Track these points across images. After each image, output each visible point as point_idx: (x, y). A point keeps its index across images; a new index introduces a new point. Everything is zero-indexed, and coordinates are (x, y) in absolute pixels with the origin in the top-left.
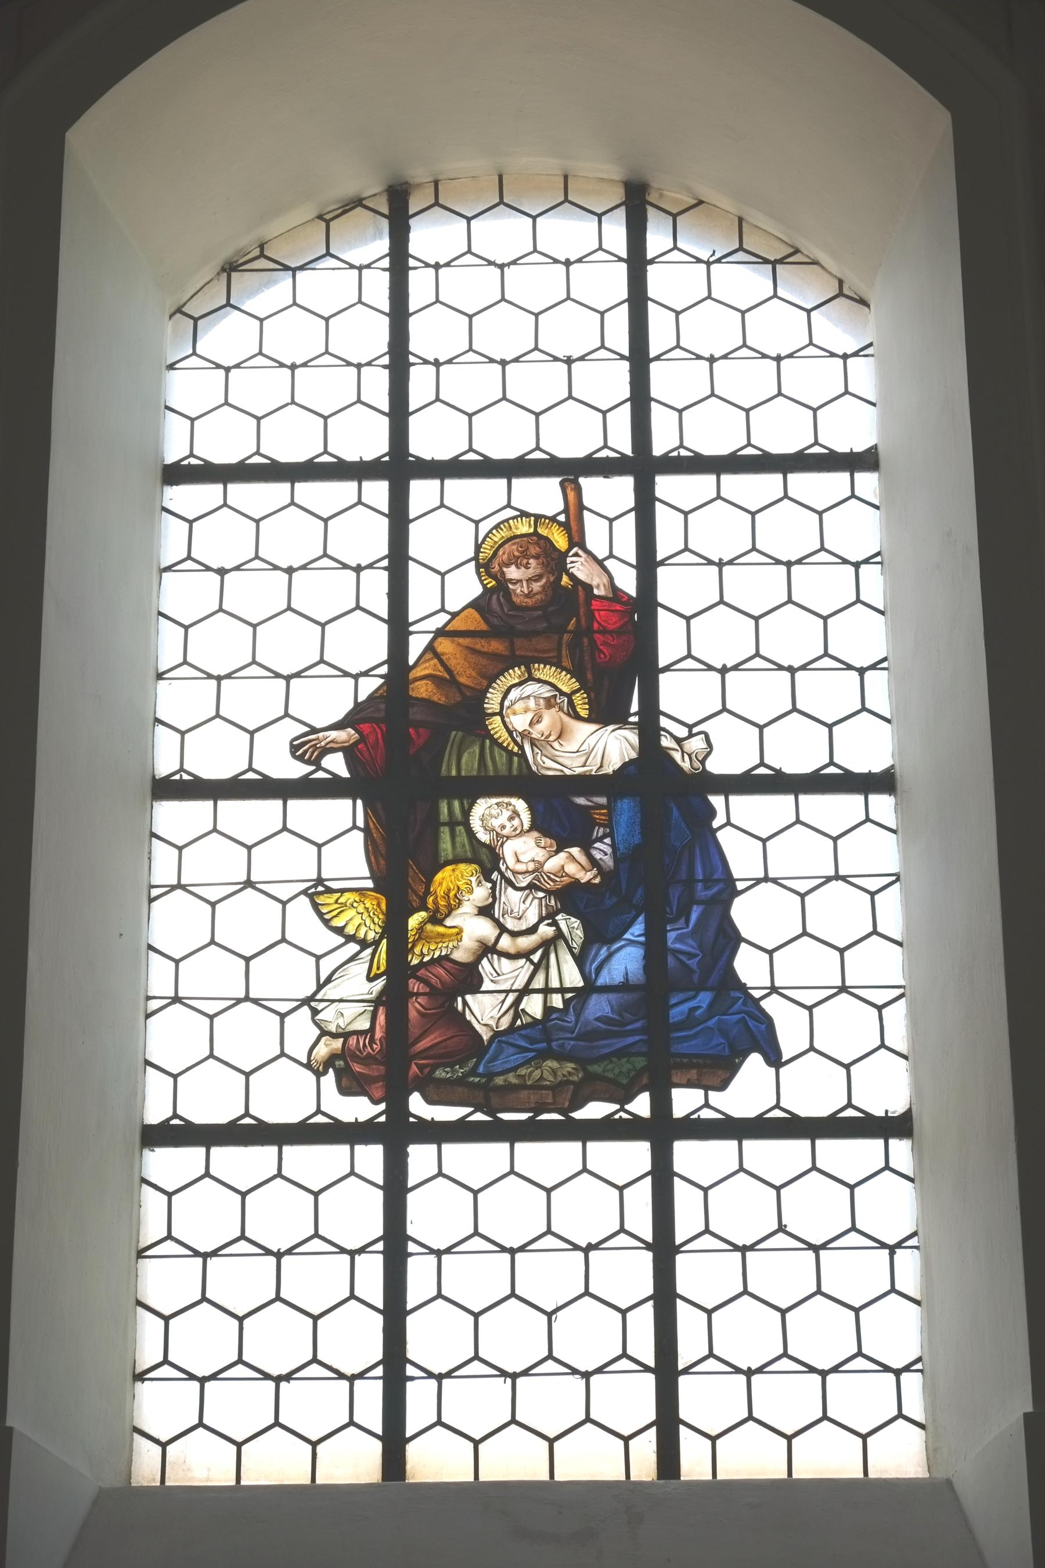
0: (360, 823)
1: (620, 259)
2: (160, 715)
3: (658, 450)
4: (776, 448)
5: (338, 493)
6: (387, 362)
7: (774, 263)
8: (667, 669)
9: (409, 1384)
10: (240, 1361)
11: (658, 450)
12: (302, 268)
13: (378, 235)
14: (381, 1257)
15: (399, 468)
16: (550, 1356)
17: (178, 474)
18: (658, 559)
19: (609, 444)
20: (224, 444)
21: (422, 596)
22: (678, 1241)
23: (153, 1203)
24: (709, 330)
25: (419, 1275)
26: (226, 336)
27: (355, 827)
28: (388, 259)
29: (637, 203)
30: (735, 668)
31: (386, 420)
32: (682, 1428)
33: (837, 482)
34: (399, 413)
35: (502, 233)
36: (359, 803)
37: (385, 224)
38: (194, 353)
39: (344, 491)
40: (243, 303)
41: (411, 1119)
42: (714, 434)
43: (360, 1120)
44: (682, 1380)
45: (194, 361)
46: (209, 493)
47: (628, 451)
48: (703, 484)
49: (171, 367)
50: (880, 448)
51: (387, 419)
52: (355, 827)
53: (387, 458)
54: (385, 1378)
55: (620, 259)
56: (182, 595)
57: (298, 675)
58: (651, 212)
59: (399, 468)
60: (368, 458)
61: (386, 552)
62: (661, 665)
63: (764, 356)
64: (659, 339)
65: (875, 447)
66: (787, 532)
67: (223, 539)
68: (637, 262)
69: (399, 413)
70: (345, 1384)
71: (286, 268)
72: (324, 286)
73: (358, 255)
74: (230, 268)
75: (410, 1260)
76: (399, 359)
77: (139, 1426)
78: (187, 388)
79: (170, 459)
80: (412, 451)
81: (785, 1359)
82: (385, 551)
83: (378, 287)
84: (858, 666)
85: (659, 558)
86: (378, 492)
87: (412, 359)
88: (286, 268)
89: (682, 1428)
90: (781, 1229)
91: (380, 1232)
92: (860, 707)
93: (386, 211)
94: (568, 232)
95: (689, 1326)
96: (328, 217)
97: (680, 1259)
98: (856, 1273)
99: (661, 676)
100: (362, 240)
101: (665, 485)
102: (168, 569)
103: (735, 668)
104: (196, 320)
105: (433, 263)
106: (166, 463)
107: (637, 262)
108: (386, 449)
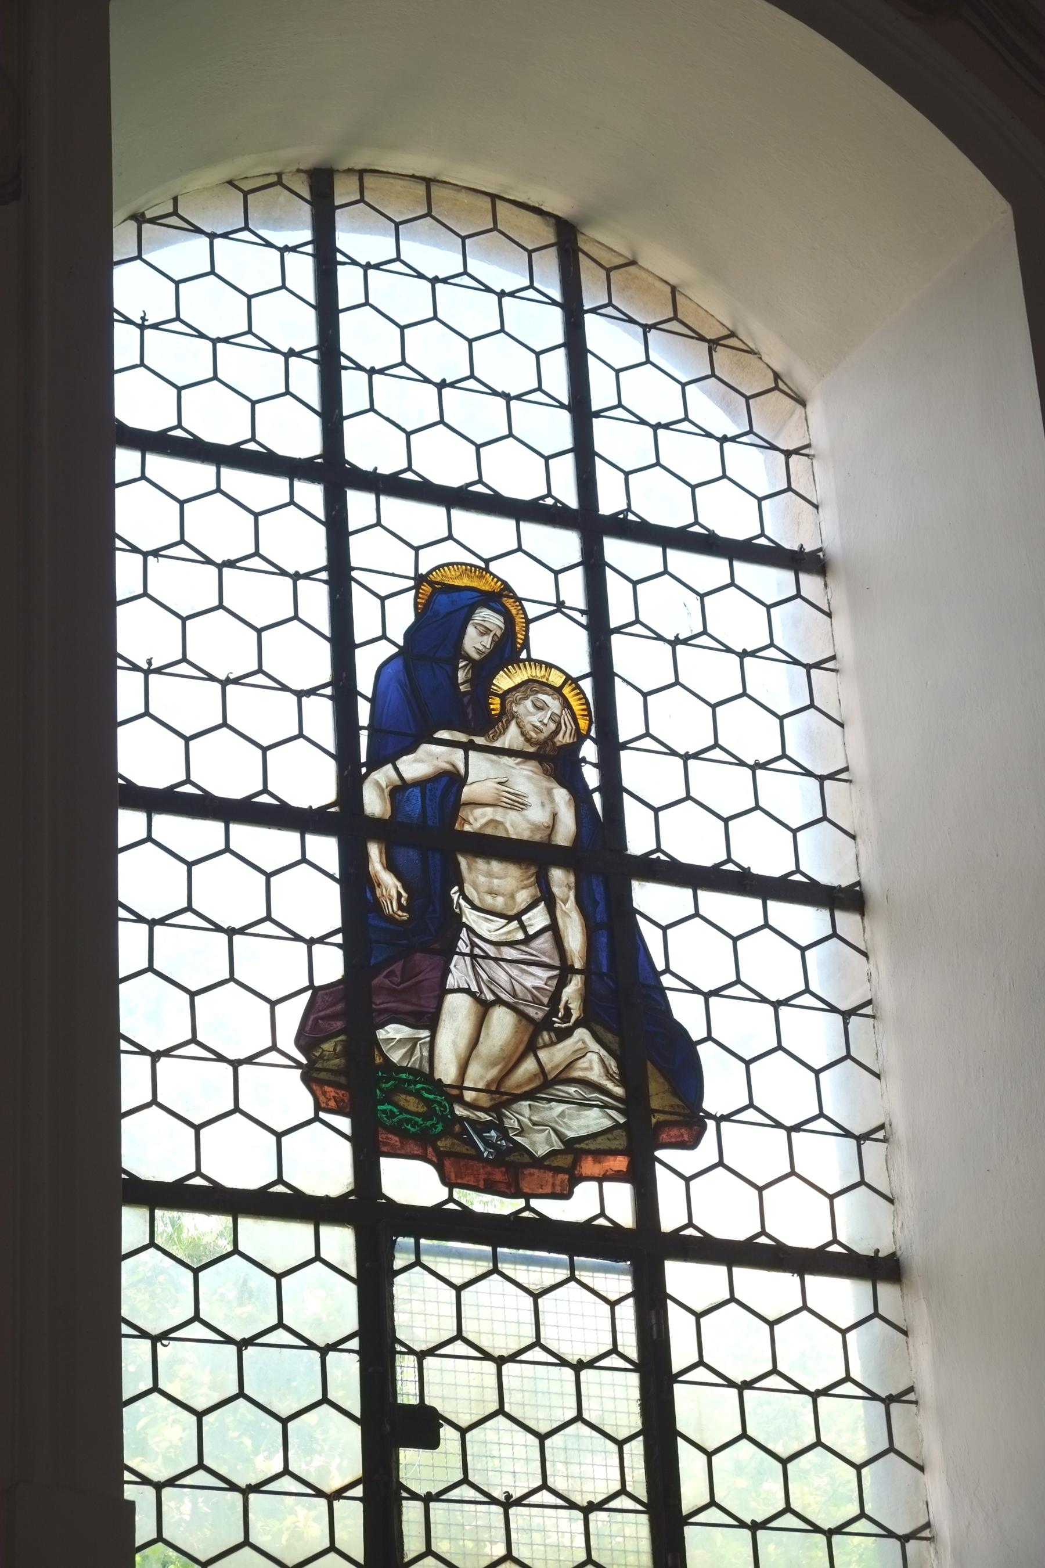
25: (353, 389)
34: (331, 415)
37: (307, 209)
63: (708, 435)
69: (331, 415)
73: (281, 238)
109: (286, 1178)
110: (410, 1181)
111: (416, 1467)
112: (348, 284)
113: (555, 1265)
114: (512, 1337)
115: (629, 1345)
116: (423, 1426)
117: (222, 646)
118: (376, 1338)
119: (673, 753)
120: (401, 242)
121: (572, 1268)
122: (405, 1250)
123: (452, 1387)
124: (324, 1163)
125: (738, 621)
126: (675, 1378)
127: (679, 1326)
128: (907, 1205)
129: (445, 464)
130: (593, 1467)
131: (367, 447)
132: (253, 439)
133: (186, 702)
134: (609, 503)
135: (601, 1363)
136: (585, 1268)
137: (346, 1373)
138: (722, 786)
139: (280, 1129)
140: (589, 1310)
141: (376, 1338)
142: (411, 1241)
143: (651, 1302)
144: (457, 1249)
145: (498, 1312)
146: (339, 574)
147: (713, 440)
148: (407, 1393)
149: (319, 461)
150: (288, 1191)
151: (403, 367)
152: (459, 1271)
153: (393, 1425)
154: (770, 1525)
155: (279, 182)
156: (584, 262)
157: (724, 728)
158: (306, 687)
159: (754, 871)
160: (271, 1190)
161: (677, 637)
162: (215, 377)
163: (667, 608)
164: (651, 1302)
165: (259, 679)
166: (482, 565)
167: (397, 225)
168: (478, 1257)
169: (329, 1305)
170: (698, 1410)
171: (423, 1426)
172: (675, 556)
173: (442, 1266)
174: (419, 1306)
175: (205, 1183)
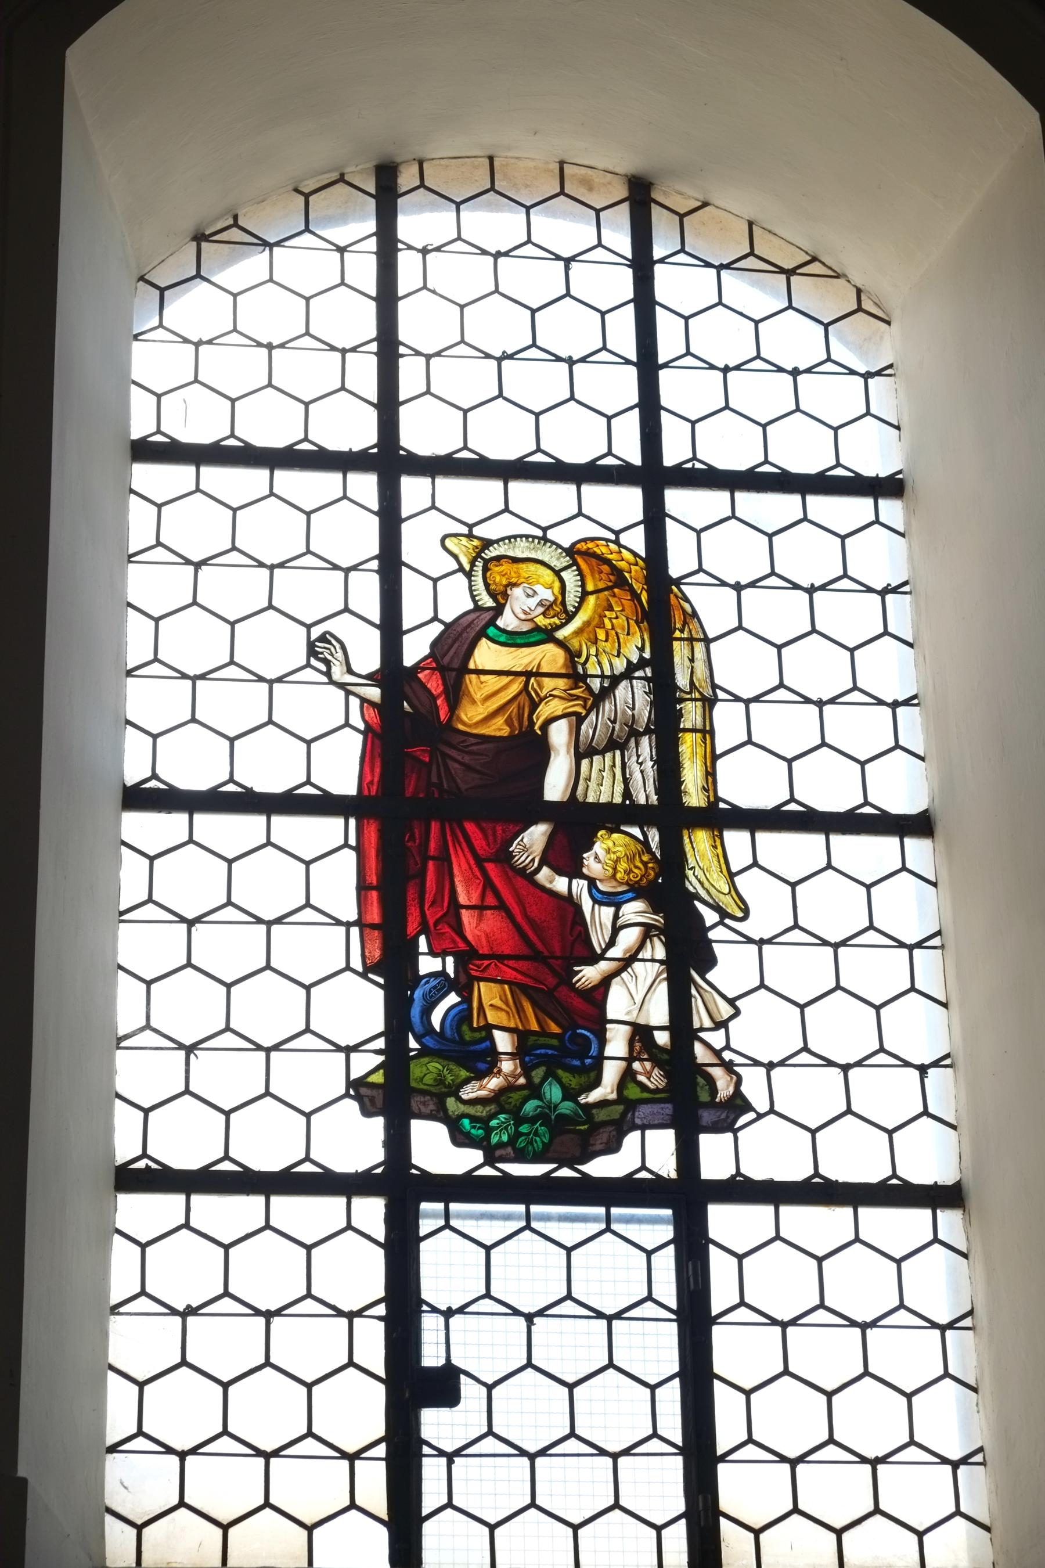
0: (352, 841)
1: (628, 362)
2: (130, 717)
3: (670, 459)
4: (796, 467)
5: (324, 484)
6: (383, 1047)
7: (790, 273)
8: (666, 365)
9: (400, 360)
10: (226, 1294)
11: (670, 459)
12: (278, 244)
13: (363, 218)
14: (374, 359)
15: (389, 461)
16: (572, 1434)
17: (146, 451)
18: (719, 1454)
19: (614, 451)
20: (193, 767)
21: (415, 606)
22: (714, 1312)
23: (123, 1257)
24: (722, 338)
25: (410, 375)
26: (195, 309)
27: (346, 845)
28: (375, 344)
29: (640, 197)
30: (738, 368)
31: (373, 305)
32: (716, 1382)
33: (860, 508)
34: (388, 405)
35: (494, 225)
36: (352, 822)
37: (372, 203)
38: (161, 325)
39: (329, 482)
40: (215, 274)
41: (401, 452)
42: (730, 448)
43: (354, 450)
44: (663, 374)
45: (160, 334)
46: (182, 475)
47: (636, 460)
48: (716, 501)
49: (136, 337)
50: (964, 1182)
51: (373, 304)
52: (346, 845)
53: (375, 450)
54: (390, 1460)
55: (628, 362)
56: (149, 585)
57: (282, 565)
58: (655, 210)
59: (389, 461)
60: (356, 449)
61: (381, 1293)
62: (661, 361)
63: (780, 369)
64: (668, 344)
65: (926, 811)
66: (808, 556)
67: (196, 527)
68: (642, 266)
69: (388, 405)
70: (344, 1321)
71: (265, 244)
72: (304, 263)
73: (341, 234)
74: (200, 238)
75: (399, 254)
76: (388, 347)
77: (122, 964)
78: (152, 362)
79: (135, 435)
80: (415, 1161)
81: (821, 1311)
82: (373, 333)
83: (364, 270)
84: (918, 1062)
85: (719, 1452)
86: (371, 1212)
87: (400, 246)
88: (265, 244)
89: (716, 1382)
90: (805, 1049)
91: (381, 1432)
92: (893, 744)
93: (373, 191)
94: (564, 230)
95: (726, 1406)
96: (307, 187)
97: (716, 1330)
98: (876, 971)
99: (661, 372)
100: (342, 219)
101: (675, 499)
102: (113, 1449)
103: (738, 368)
104: (162, 291)
105: (444, 1308)
106: (117, 1164)
107: (642, 266)
108: (374, 440)
109: (899, 1173)
110: (433, 1149)
111: (436, 1425)
112: (408, 269)
113: (507, 1217)
114: (545, 1293)
115: (667, 1291)
116: (445, 1386)
117: (817, 669)
118: (403, 1303)
119: (880, 702)
120: (602, 230)
121: (528, 1217)
122: (433, 1215)
123: (473, 1345)
124: (355, 1142)
125: (808, 556)
126: (714, 1320)
127: (721, 1270)
128: (963, 1127)
129: (502, 438)
130: (616, 1412)
131: (423, 432)
132: (609, 453)
133: (786, 726)
134: (674, 451)
135: (549, 1312)
136: (546, 1218)
137: (372, 1342)
138: (232, 704)
139: (146, 1105)
140: (625, 1260)
141: (403, 1303)
142: (440, 1206)
143: (692, 1248)
144: (650, 1216)
145: (529, 1268)
146: (390, 563)
147: (784, 374)
148: (432, 1357)
149: (375, 450)
150: (320, 1170)
151: (689, 357)
152: (570, 1234)
153: (416, 1386)
154: (201, 1451)
155: (342, 179)
156: (656, 211)
157: (816, 665)
158: (199, 672)
159: (257, 789)
160: (132, 1166)
161: (812, 585)
162: (798, 409)
163: (735, 553)
164: (692, 1248)
165: (856, 697)
166: (613, 537)
167: (598, 212)
168: (595, 1219)
169: (359, 1273)
170: (735, 1351)
171: (445, 1386)
172: (208, 472)
173: (630, 1231)
174: (446, 1267)
175: (649, 1176)
